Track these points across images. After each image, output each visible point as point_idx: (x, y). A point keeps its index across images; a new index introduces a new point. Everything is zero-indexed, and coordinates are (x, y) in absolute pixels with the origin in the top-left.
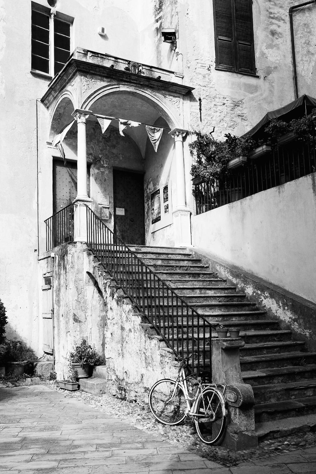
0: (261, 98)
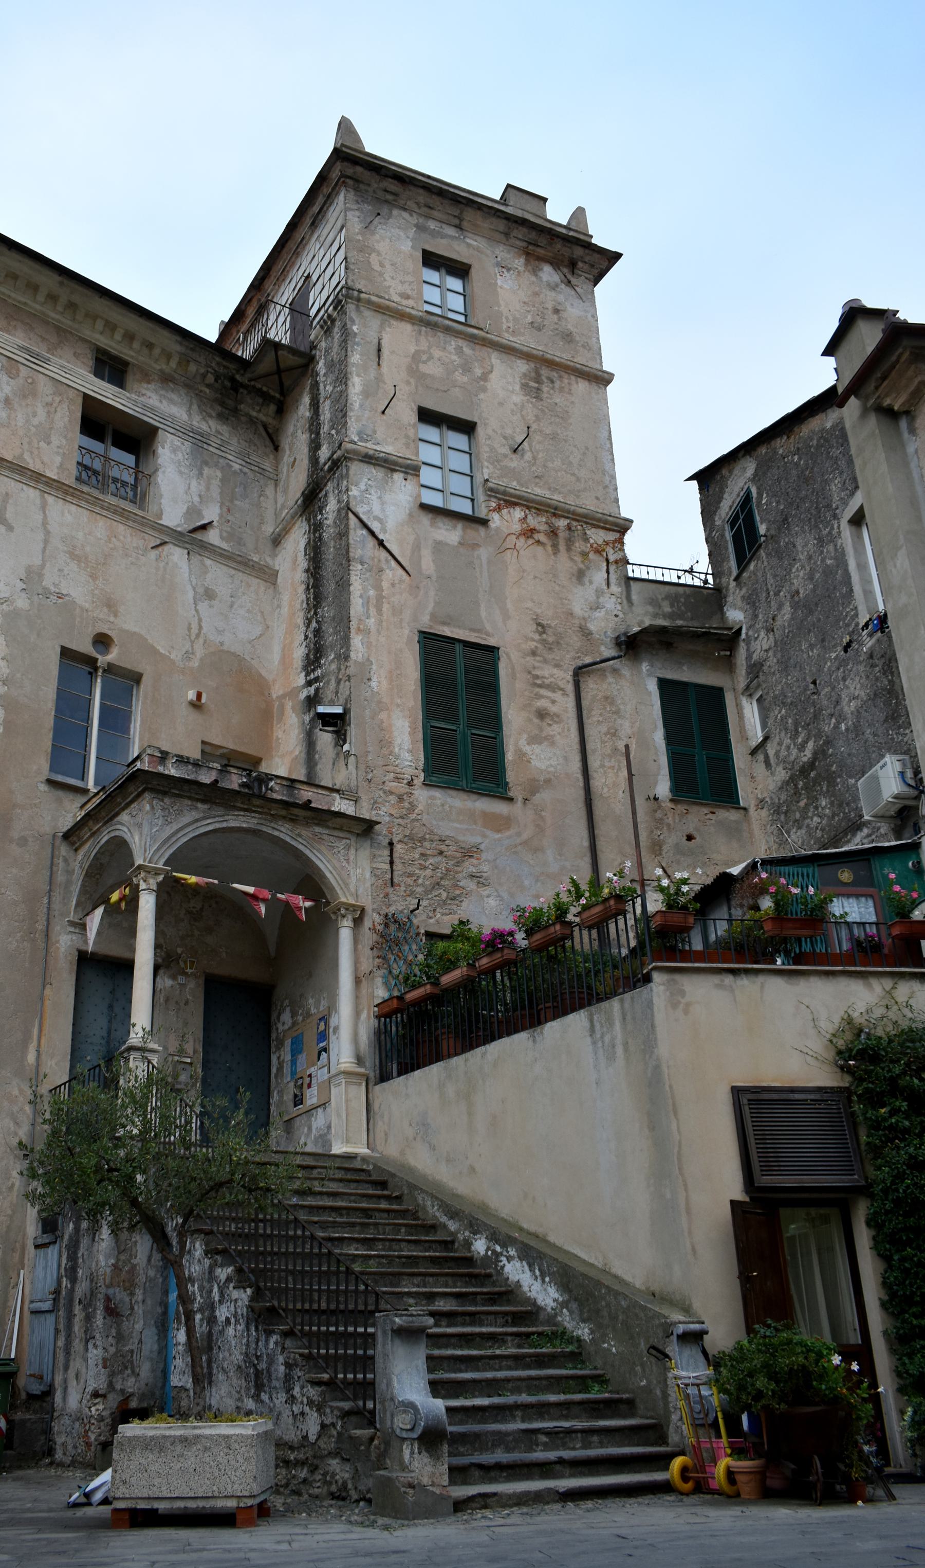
0: (518, 841)
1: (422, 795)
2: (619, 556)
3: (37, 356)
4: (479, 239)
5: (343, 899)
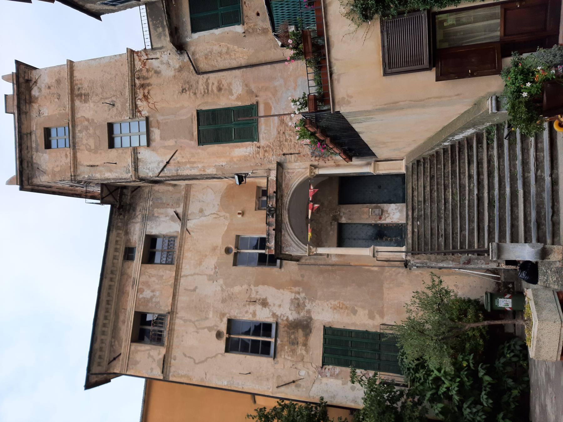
1: (263, 143)
2: (143, 53)
3: (134, 282)
4: (32, 125)
5: (308, 174)
